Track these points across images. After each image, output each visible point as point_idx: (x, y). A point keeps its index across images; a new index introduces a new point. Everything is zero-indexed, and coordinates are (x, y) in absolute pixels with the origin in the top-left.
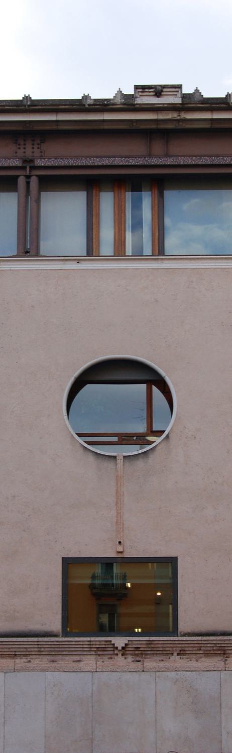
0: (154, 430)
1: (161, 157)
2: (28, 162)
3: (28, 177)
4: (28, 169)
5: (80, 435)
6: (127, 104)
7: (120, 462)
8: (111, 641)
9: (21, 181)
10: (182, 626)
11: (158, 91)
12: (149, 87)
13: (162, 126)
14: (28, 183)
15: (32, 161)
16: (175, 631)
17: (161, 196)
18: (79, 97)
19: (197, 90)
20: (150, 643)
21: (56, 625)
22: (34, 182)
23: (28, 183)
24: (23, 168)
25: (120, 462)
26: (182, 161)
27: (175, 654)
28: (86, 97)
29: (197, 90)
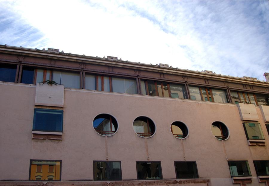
0: (112, 131)
1: (53, 64)
2: (228, 87)
3: (20, 65)
4: (20, 63)
5: (137, 133)
6: (106, 60)
7: (106, 137)
8: (40, 179)
9: (81, 73)
10: (123, 178)
11: (112, 58)
12: (111, 57)
13: (23, 54)
14: (20, 67)
15: (84, 69)
16: (121, 179)
17: (111, 80)
18: (82, 55)
19: (62, 51)
20: (116, 182)
21: (92, 178)
22: (84, 73)
23: (20, 67)
24: (19, 63)
25: (106, 137)
26: (210, 85)
27: (122, 185)
28: (6, 45)
29: (62, 51)
